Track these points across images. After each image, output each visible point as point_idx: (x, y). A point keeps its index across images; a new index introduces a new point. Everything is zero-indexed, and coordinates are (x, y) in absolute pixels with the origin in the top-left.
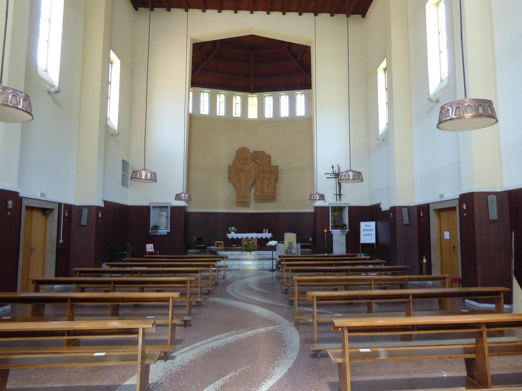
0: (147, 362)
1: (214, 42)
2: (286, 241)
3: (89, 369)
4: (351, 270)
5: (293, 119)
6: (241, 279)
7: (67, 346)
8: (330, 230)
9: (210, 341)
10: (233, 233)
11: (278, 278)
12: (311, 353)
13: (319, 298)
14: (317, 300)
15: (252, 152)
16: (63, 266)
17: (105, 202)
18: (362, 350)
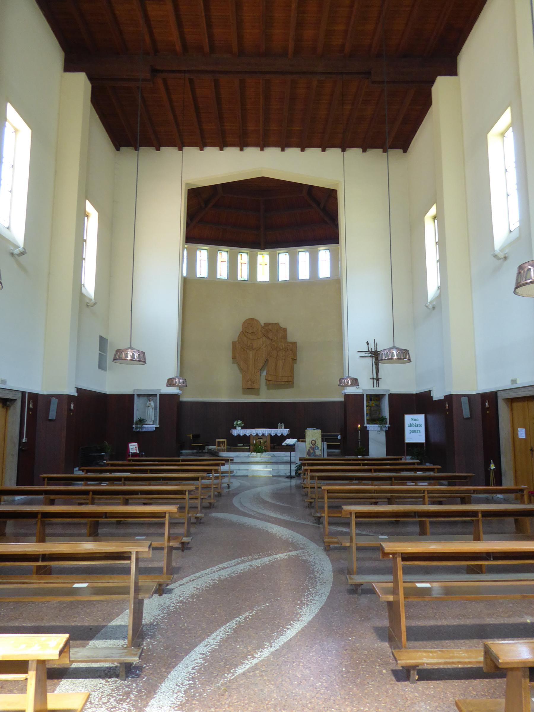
0: (140, 596)
1: (215, 187)
2: (308, 439)
3: (65, 605)
4: (396, 478)
5: (315, 281)
6: (249, 488)
7: (36, 574)
8: (366, 425)
9: (215, 570)
10: (239, 429)
11: (298, 487)
12: (349, 587)
13: (359, 515)
14: (356, 517)
15: (263, 325)
16: (27, 472)
17: (78, 390)
18: (419, 585)
